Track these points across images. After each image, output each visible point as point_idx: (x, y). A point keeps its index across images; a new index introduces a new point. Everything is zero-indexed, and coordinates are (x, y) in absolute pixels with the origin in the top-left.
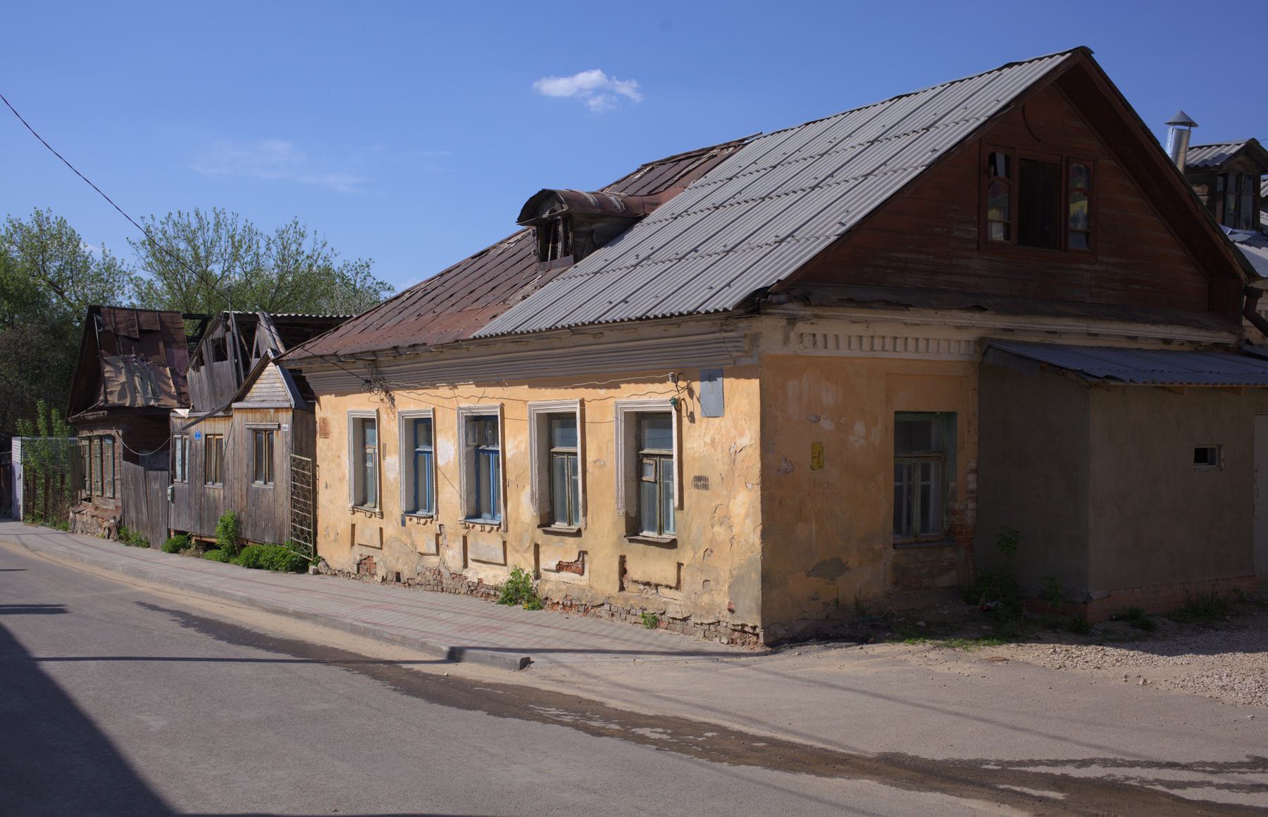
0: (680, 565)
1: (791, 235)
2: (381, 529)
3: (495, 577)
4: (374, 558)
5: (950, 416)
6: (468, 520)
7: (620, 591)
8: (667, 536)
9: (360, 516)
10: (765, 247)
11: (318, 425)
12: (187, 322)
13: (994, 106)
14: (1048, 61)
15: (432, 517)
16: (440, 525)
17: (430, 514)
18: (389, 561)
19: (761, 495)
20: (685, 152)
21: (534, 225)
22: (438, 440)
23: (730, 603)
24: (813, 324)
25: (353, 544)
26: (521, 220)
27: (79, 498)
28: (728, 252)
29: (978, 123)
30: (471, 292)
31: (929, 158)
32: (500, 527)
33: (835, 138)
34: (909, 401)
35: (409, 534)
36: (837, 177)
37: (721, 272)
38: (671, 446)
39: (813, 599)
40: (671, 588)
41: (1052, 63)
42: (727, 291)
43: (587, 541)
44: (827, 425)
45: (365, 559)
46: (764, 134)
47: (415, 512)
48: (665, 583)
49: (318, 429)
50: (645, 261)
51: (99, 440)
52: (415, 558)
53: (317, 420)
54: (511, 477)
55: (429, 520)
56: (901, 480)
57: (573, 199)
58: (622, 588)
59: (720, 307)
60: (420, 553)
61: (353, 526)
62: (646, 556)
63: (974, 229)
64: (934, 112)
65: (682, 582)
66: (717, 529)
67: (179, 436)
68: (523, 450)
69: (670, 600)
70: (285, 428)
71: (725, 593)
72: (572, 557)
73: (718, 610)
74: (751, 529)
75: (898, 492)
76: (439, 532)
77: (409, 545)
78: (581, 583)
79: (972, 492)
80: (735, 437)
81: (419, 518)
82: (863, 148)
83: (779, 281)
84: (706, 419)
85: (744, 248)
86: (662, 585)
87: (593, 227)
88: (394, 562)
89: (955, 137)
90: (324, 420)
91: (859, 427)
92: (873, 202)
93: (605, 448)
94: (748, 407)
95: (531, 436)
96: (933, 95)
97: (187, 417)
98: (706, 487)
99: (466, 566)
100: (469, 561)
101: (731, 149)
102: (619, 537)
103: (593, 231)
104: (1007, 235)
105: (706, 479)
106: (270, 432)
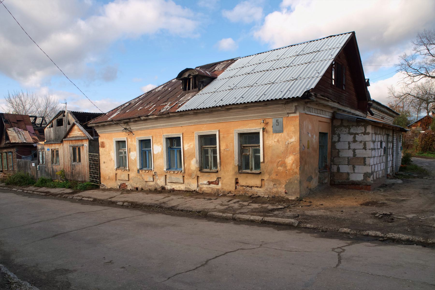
2: (129, 175)
3: (179, 187)
9: (119, 172)
15: (152, 170)
35: (141, 176)
49: (100, 145)
51: (5, 153)
52: (144, 183)
55: (150, 171)
58: (236, 188)
61: (116, 174)
62: (247, 178)
68: (192, 147)
72: (214, 179)
73: (280, 193)
74: (295, 167)
78: (217, 188)
84: (275, 134)
90: (103, 143)
93: (229, 145)
99: (166, 184)
100: (167, 183)
102: (236, 173)
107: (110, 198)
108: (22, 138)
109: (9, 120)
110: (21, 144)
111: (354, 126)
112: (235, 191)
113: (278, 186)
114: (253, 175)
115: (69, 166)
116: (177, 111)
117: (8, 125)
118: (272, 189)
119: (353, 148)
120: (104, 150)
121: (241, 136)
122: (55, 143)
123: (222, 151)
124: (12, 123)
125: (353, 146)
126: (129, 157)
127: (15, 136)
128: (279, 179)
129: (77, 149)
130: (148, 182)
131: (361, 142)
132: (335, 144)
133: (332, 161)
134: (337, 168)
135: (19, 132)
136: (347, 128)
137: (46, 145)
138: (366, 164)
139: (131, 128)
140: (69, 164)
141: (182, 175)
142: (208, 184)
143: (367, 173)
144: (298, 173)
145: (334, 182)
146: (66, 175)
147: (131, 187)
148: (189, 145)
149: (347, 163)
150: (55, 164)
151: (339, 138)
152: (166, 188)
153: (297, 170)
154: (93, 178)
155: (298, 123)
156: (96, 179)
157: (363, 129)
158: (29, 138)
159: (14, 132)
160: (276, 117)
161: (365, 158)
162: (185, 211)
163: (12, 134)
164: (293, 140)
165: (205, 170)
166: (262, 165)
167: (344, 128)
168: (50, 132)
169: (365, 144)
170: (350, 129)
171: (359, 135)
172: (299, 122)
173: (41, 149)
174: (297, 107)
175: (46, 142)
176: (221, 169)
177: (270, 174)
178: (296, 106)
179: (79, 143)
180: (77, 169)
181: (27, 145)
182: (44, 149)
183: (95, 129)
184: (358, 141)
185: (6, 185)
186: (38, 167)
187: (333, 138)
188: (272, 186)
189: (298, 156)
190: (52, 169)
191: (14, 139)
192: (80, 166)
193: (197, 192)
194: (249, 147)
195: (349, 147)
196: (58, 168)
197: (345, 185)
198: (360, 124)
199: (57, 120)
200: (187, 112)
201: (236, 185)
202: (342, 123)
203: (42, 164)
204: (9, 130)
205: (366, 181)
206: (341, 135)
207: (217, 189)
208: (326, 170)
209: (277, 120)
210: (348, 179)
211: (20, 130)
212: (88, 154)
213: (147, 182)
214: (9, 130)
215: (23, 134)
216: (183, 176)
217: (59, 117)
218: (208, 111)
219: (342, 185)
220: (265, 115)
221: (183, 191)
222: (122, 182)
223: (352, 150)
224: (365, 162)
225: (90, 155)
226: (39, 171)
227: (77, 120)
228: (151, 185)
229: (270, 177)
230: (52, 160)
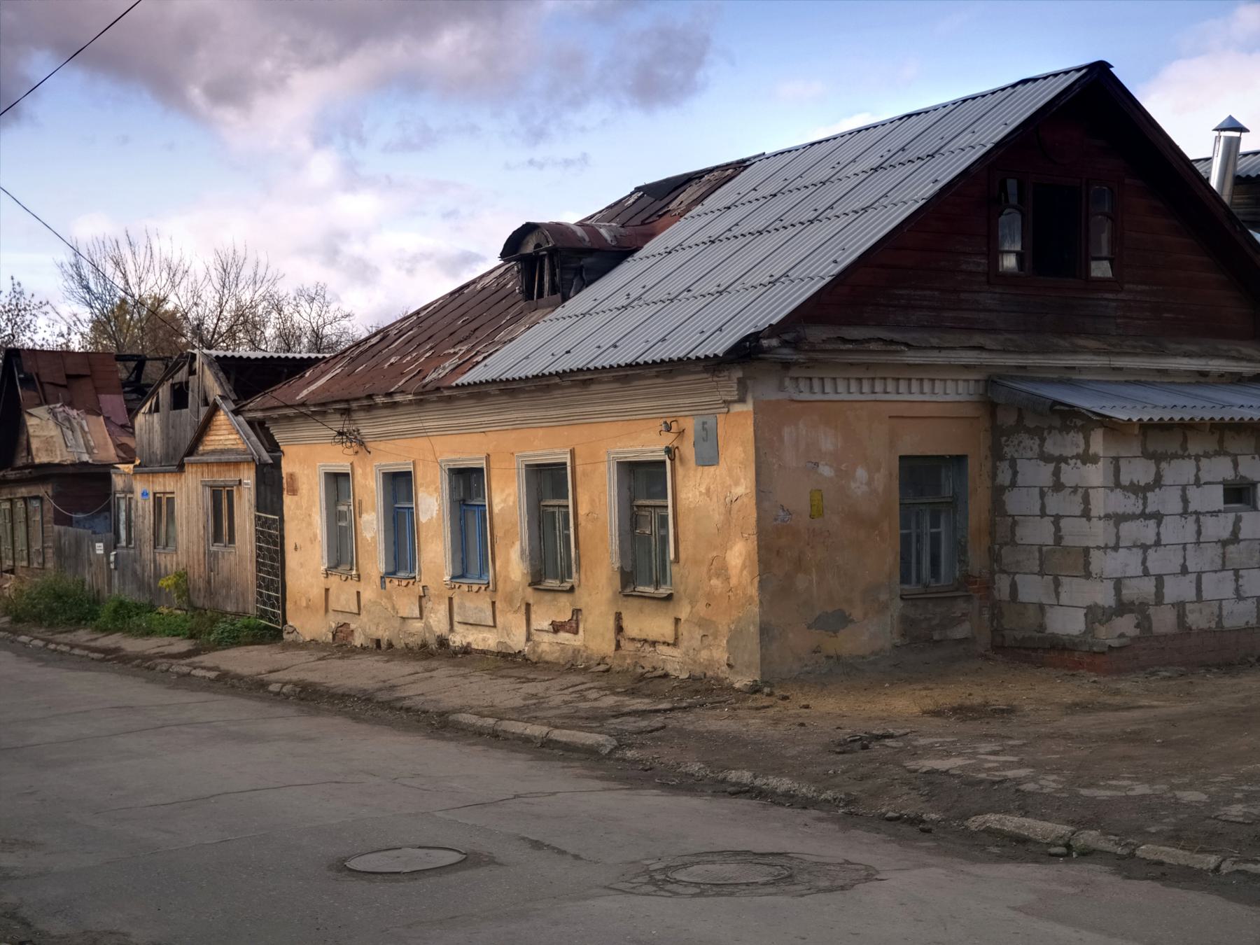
0: (677, 620)
1: (786, 275)
2: (358, 593)
3: (484, 640)
5: (960, 460)
6: (454, 580)
7: (616, 650)
8: (664, 591)
9: (334, 581)
10: (759, 288)
11: (284, 481)
12: (119, 365)
13: (1003, 130)
14: (1063, 77)
15: (415, 578)
16: (423, 587)
17: (412, 575)
18: (367, 627)
19: (758, 545)
22: (420, 495)
23: (728, 658)
24: (808, 367)
26: (503, 255)
28: (721, 293)
29: (984, 150)
30: (451, 334)
31: (929, 190)
32: (488, 586)
33: (839, 163)
34: (915, 443)
35: (390, 598)
36: (838, 210)
37: (679, 342)
38: (666, 497)
39: (815, 652)
41: (1066, 80)
42: (718, 335)
43: (583, 598)
44: (826, 471)
45: (341, 626)
47: (394, 573)
48: (662, 639)
49: (285, 486)
50: (636, 302)
51: (23, 502)
52: (397, 623)
53: (284, 475)
54: (499, 532)
55: (412, 581)
56: (910, 528)
57: (558, 230)
58: (618, 646)
59: (710, 353)
60: (402, 617)
61: (327, 590)
62: (642, 612)
63: (983, 261)
65: (680, 638)
66: (714, 582)
67: (123, 495)
68: (511, 504)
69: (669, 658)
70: (247, 484)
72: (566, 616)
73: (717, 666)
74: (749, 580)
75: (905, 540)
76: (422, 594)
78: (576, 643)
80: (730, 486)
81: (400, 579)
82: (866, 175)
83: (771, 325)
84: (700, 468)
85: (738, 289)
86: (659, 642)
87: (582, 263)
88: (373, 628)
89: (953, 170)
90: (292, 476)
91: (861, 473)
92: (957, 168)
93: (597, 500)
94: (743, 455)
95: (519, 489)
96: (944, 114)
99: (452, 629)
100: (455, 624)
102: (614, 593)
107: (270, 672)
108: (78, 446)
109: (37, 375)
110: (71, 468)
111: (1055, 428)
112: (615, 657)
113: (712, 642)
114: (655, 602)
115: (201, 556)
116: (454, 384)
117: (34, 394)
118: (699, 651)
119: (1054, 514)
120: (297, 502)
121: (630, 471)
122: (165, 472)
123: (581, 519)
124: (48, 389)
125: (1055, 504)
126: (358, 532)
127: (52, 437)
128: (714, 619)
129: (224, 495)
130: (410, 621)
131: (1075, 489)
132: (1004, 494)
133: (994, 557)
134: (1011, 586)
135: (69, 421)
136: (1036, 438)
137: (138, 477)
138: (1091, 573)
139: (361, 431)
140: (202, 550)
141: (491, 598)
142: (552, 630)
143: (1096, 605)
144: (757, 599)
145: (1003, 636)
146: (191, 591)
147: (363, 636)
148: (504, 496)
149: (1037, 569)
150: (164, 549)
151: (1015, 473)
152: (451, 643)
153: (753, 591)
154: (265, 604)
155: (752, 434)
156: (273, 606)
157: (1080, 438)
158: (106, 444)
159: (51, 423)
160: (700, 412)
161: (1086, 551)
162: (414, 711)
163: (42, 429)
164: (740, 490)
165: (551, 583)
166: (674, 570)
167: (1027, 436)
168: (150, 430)
169: (1086, 500)
170: (1043, 440)
171: (1068, 464)
172: (755, 431)
173: (123, 492)
174: (749, 382)
175: (140, 465)
176: (580, 581)
177: (693, 603)
178: (741, 382)
179: (228, 476)
180: (222, 567)
181: (93, 470)
182: (132, 492)
183: (268, 428)
184: (1067, 485)
185: (11, 622)
186: (112, 558)
187: (998, 472)
188: (699, 643)
189: (753, 543)
190: (155, 566)
191: (47, 450)
192: (232, 558)
193: (526, 659)
194: (650, 509)
195: (1043, 507)
196: (169, 561)
197: (1035, 650)
198: (1071, 421)
199: (173, 385)
200: (483, 389)
201: (619, 637)
202: (1020, 417)
203: (127, 546)
204: (31, 415)
205: (1093, 637)
206: (1018, 461)
207: (575, 650)
208: (967, 591)
209: (704, 423)
210: (1042, 628)
211: (74, 412)
212: (253, 517)
213: (407, 621)
214: (31, 415)
215: (82, 427)
216: (493, 603)
217: (176, 376)
218: (533, 388)
219: (1026, 649)
220: (669, 406)
221: (492, 653)
222: (342, 619)
223: (1052, 519)
224: (1087, 564)
225: (258, 518)
226: (116, 574)
227: (228, 387)
228: (413, 631)
229: (694, 610)
230: (154, 535)
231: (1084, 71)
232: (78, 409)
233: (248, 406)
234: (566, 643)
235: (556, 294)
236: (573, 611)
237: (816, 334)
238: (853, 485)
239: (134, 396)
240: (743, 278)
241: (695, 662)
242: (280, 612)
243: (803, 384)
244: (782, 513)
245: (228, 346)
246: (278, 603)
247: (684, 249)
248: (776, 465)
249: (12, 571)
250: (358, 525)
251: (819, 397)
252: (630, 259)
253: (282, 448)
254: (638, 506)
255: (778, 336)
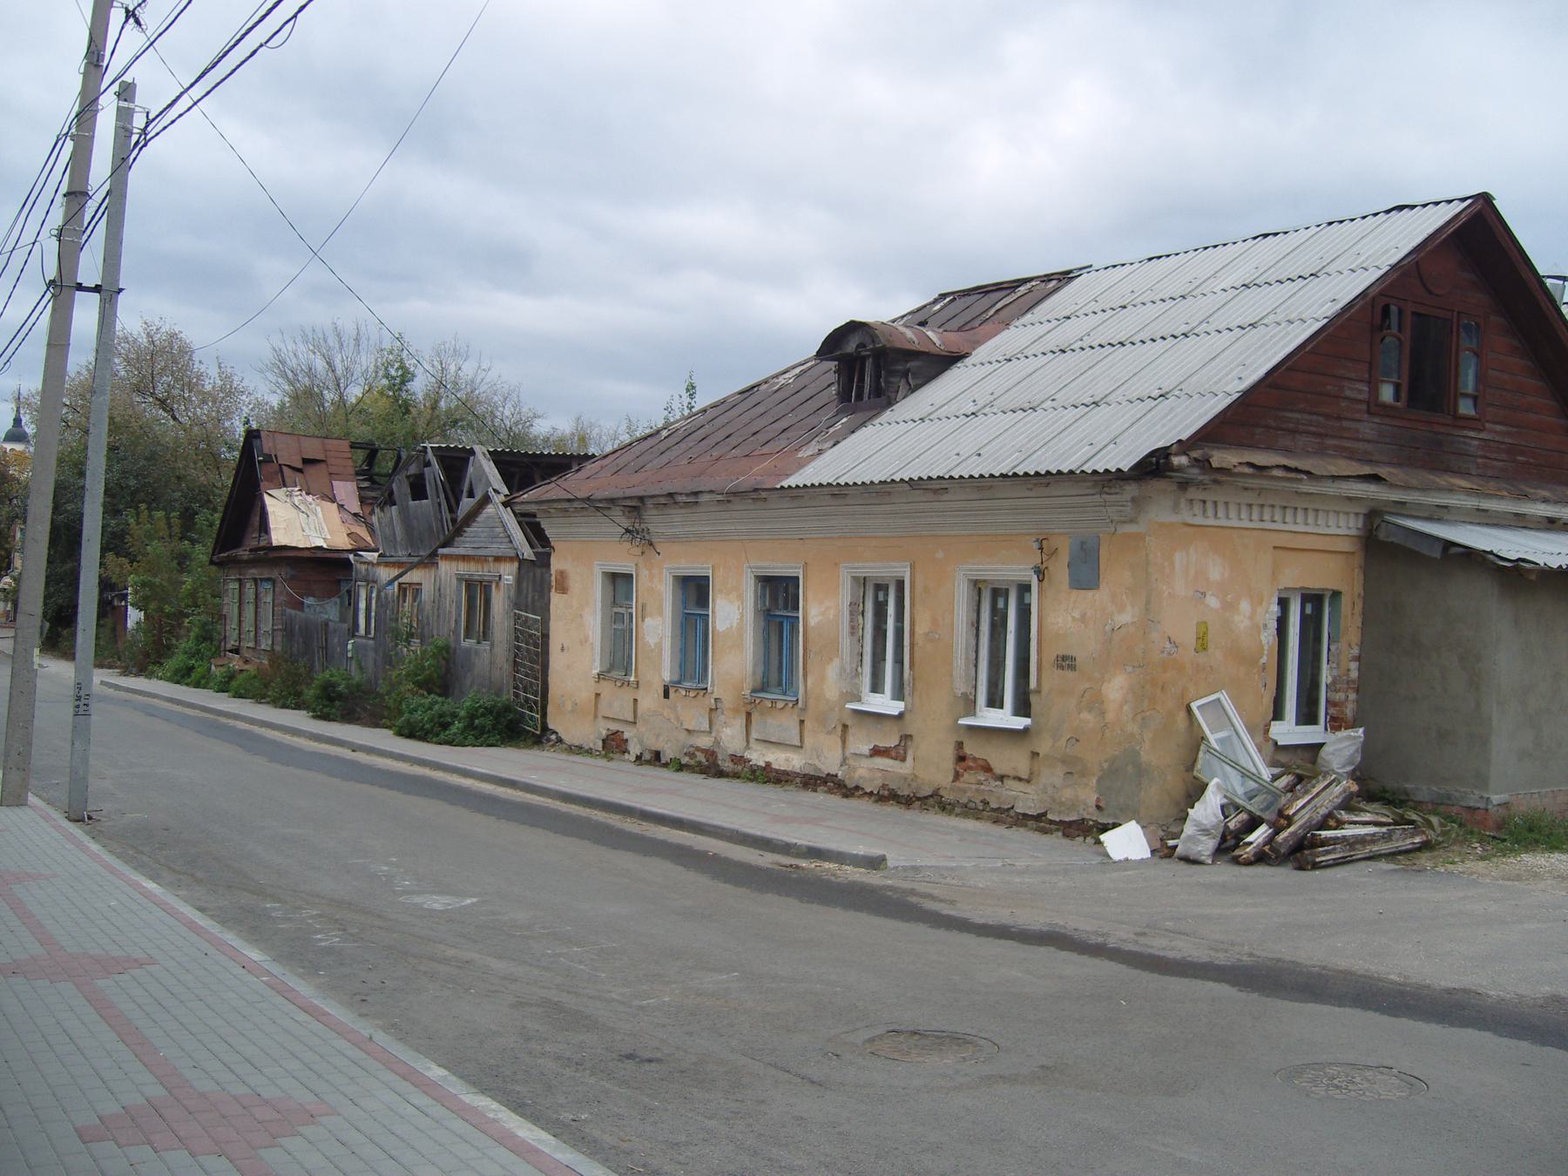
2: (635, 700)
4: (625, 733)
5: (1336, 595)
6: (755, 695)
9: (606, 688)
15: (706, 689)
16: (716, 699)
17: (702, 686)
20: (995, 281)
21: (835, 360)
23: (1098, 799)
25: (596, 717)
27: (222, 649)
30: (754, 434)
40: (1020, 779)
44: (1213, 602)
46: (1095, 268)
47: (679, 682)
48: (1012, 773)
49: (553, 583)
51: (253, 584)
53: (553, 572)
55: (702, 693)
61: (598, 695)
63: (1365, 388)
64: (1319, 255)
66: (1085, 715)
68: (831, 617)
70: (507, 580)
71: (1092, 788)
72: (891, 742)
73: (1082, 806)
74: (1131, 716)
76: (714, 707)
77: (672, 721)
79: (1353, 681)
87: (908, 365)
91: (1245, 606)
97: (375, 562)
98: (1073, 668)
101: (1054, 282)
103: (909, 370)
104: (1397, 397)
105: (1073, 659)
106: (486, 589)
109: (275, 456)
112: (952, 789)
116: (778, 486)
123: (919, 640)
126: (640, 637)
141: (798, 716)
216: (802, 722)
222: (614, 727)
231: (1469, 201)
232: (314, 495)
233: (522, 497)
234: (889, 769)
235: (880, 397)
236: (901, 737)
237: (1223, 458)
238: (1237, 618)
239: (366, 484)
240: (1124, 387)
241: (1054, 800)
242: (539, 716)
243: (1197, 508)
244: (1168, 645)
245: (112, 472)
246: (537, 707)
247: (1027, 357)
248: (1166, 593)
249: (236, 651)
250: (639, 629)
251: (1211, 522)
252: (959, 365)
253: (552, 544)
254: (781, 624)
255: (1185, 454)
